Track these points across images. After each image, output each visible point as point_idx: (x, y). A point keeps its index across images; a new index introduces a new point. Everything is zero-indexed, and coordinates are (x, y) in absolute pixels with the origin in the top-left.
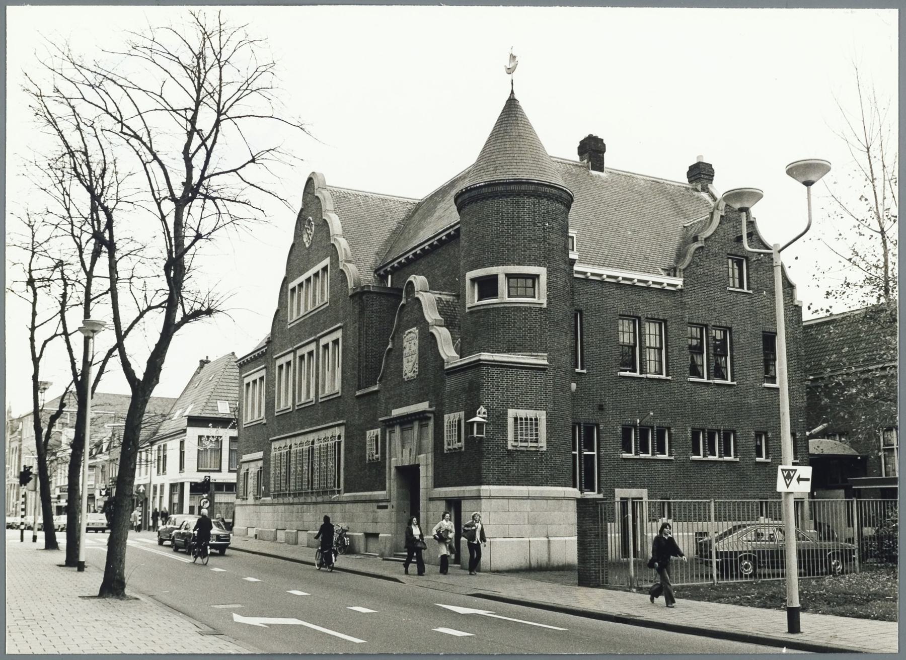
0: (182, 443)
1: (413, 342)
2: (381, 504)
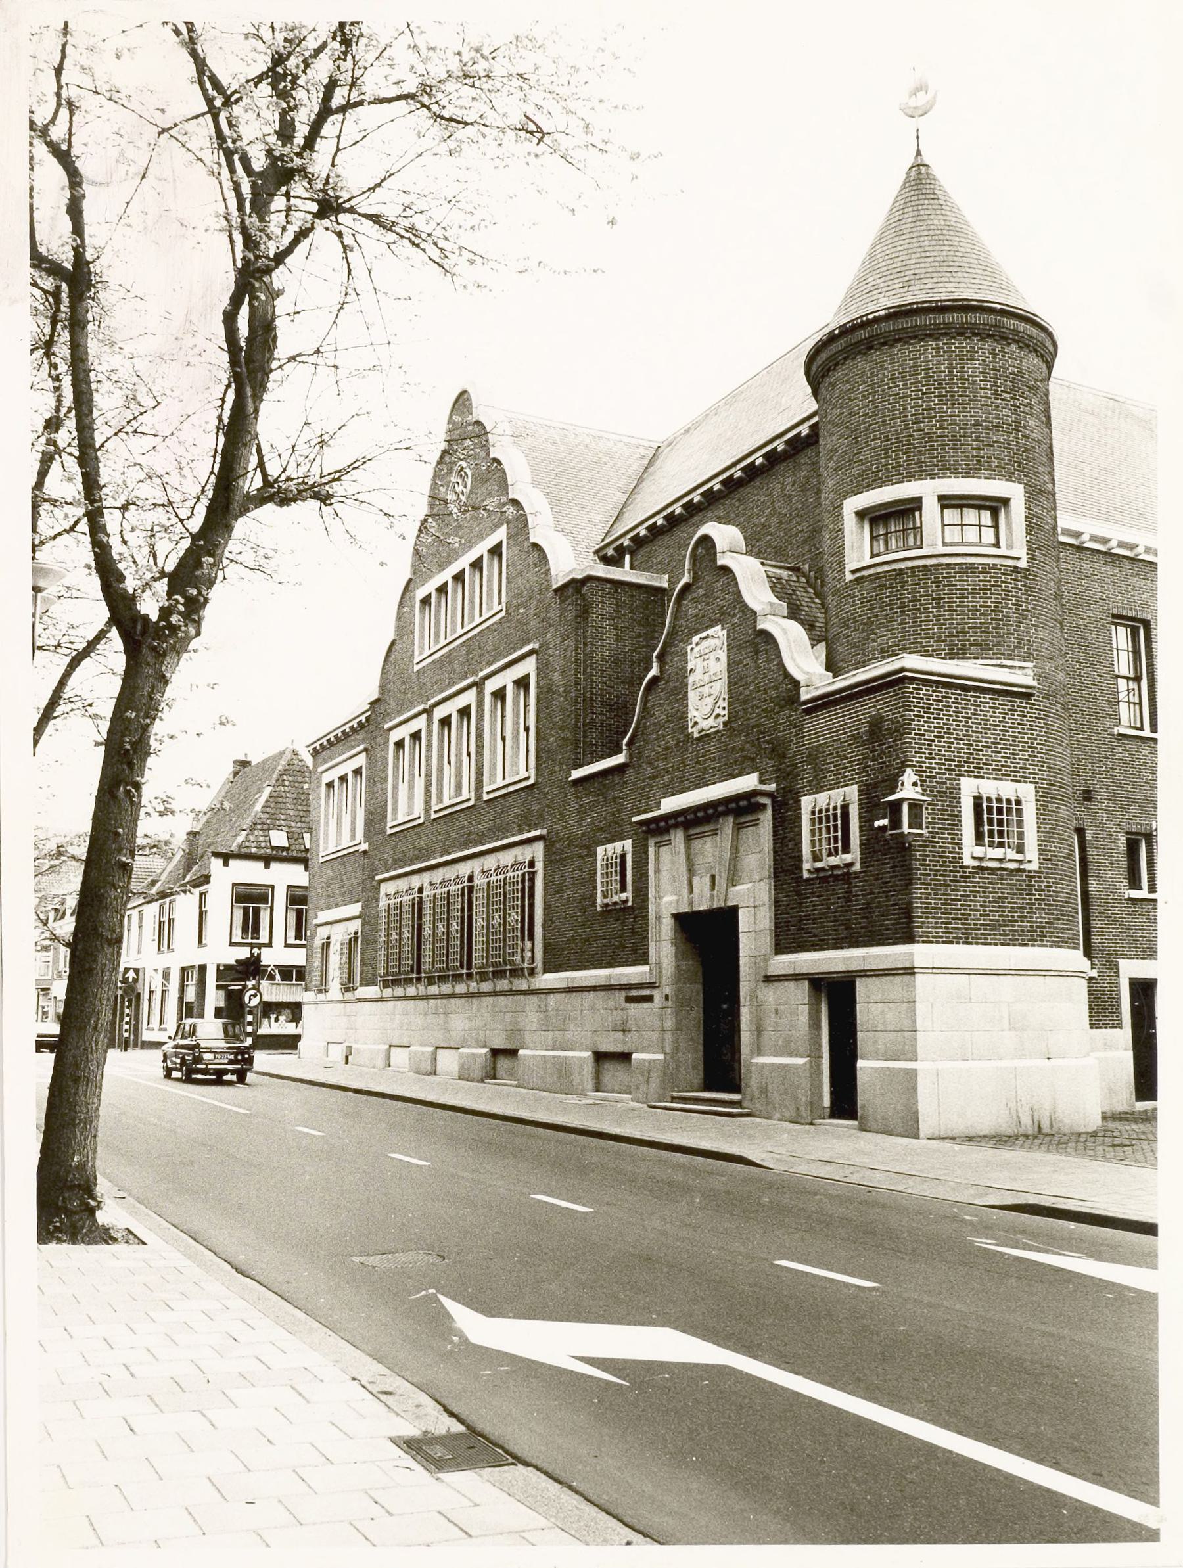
0: (203, 895)
1: (712, 656)
2: (634, 993)
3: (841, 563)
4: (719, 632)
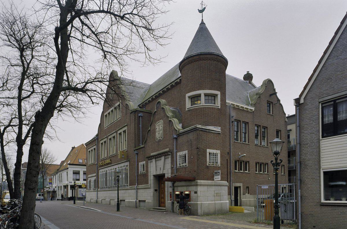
3: (185, 107)
4: (162, 121)
